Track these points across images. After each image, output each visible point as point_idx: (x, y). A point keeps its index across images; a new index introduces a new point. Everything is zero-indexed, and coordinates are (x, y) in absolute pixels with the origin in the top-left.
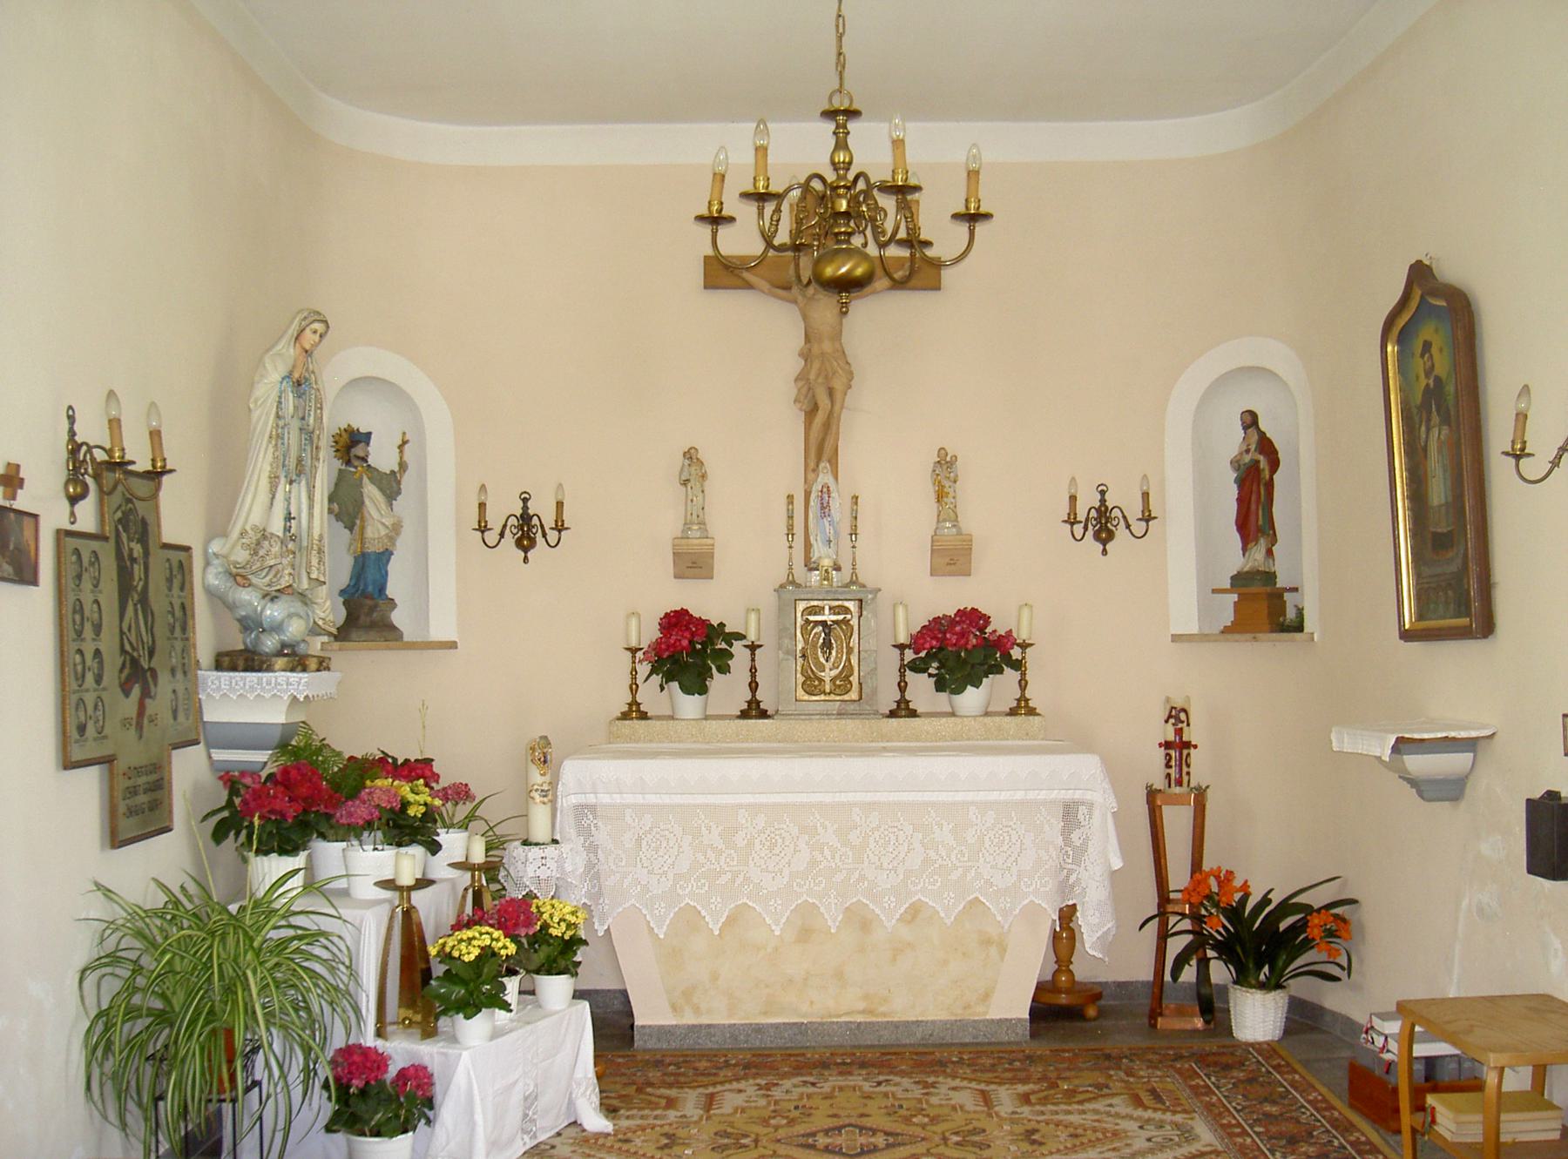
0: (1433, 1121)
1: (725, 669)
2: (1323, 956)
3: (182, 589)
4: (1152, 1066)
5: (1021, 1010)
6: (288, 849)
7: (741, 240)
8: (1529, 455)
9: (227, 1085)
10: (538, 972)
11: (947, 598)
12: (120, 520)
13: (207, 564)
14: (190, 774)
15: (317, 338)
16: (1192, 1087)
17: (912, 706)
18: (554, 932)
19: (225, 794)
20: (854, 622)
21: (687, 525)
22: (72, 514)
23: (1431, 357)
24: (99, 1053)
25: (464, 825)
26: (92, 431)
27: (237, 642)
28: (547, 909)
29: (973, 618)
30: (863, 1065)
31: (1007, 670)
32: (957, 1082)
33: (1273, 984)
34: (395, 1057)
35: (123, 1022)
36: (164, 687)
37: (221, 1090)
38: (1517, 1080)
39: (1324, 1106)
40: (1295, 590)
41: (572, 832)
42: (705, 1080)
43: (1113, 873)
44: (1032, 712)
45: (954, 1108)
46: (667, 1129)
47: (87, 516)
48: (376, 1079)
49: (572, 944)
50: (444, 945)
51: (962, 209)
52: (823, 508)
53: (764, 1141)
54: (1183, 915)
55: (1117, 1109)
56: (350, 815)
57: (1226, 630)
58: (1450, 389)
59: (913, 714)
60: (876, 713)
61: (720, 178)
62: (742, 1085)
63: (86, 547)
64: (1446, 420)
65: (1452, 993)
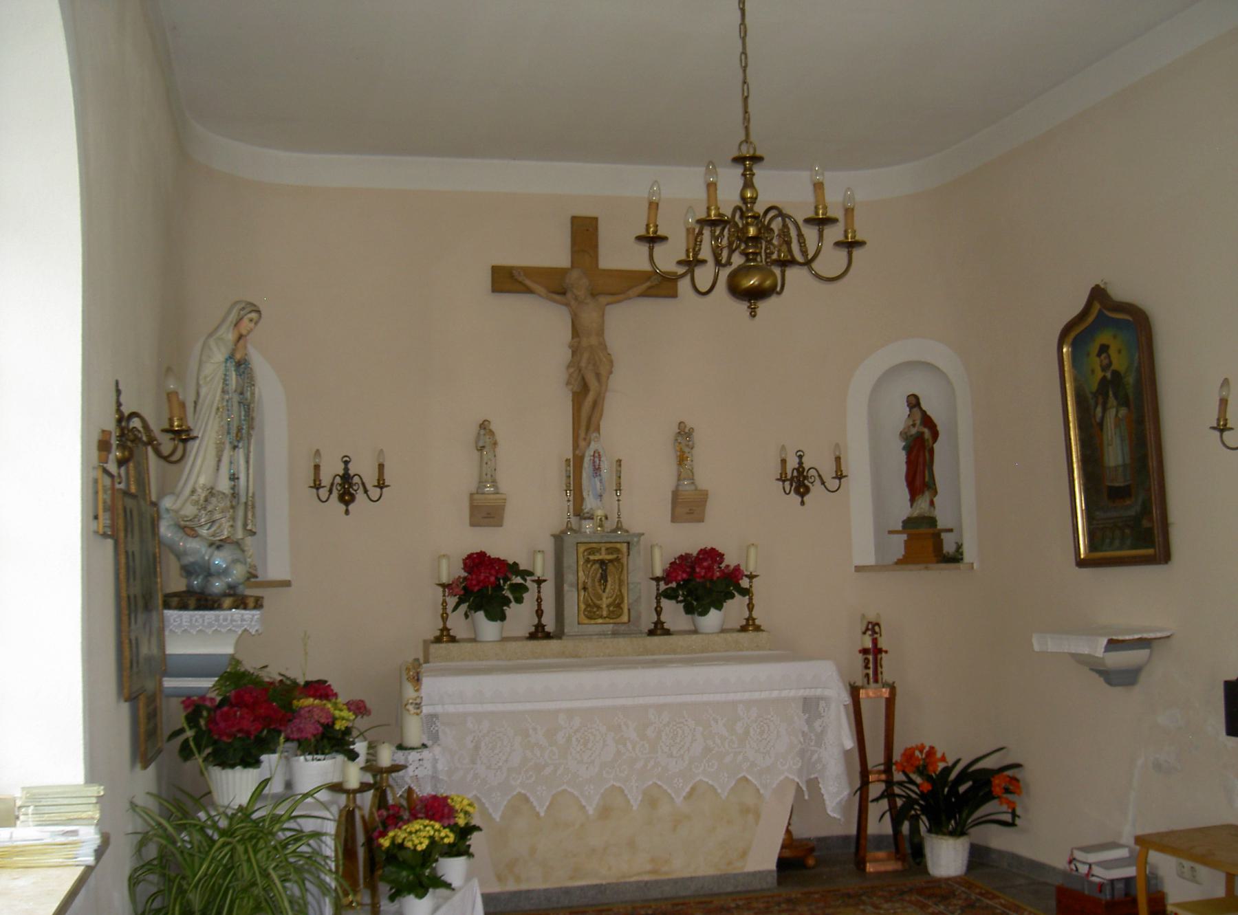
1: (519, 600)
5: (772, 865)
6: (251, 761)
11: (689, 540)
21: (481, 483)
23: (1109, 357)
29: (712, 555)
33: (959, 832)
44: (758, 629)
57: (899, 562)
59: (667, 632)
60: (641, 633)
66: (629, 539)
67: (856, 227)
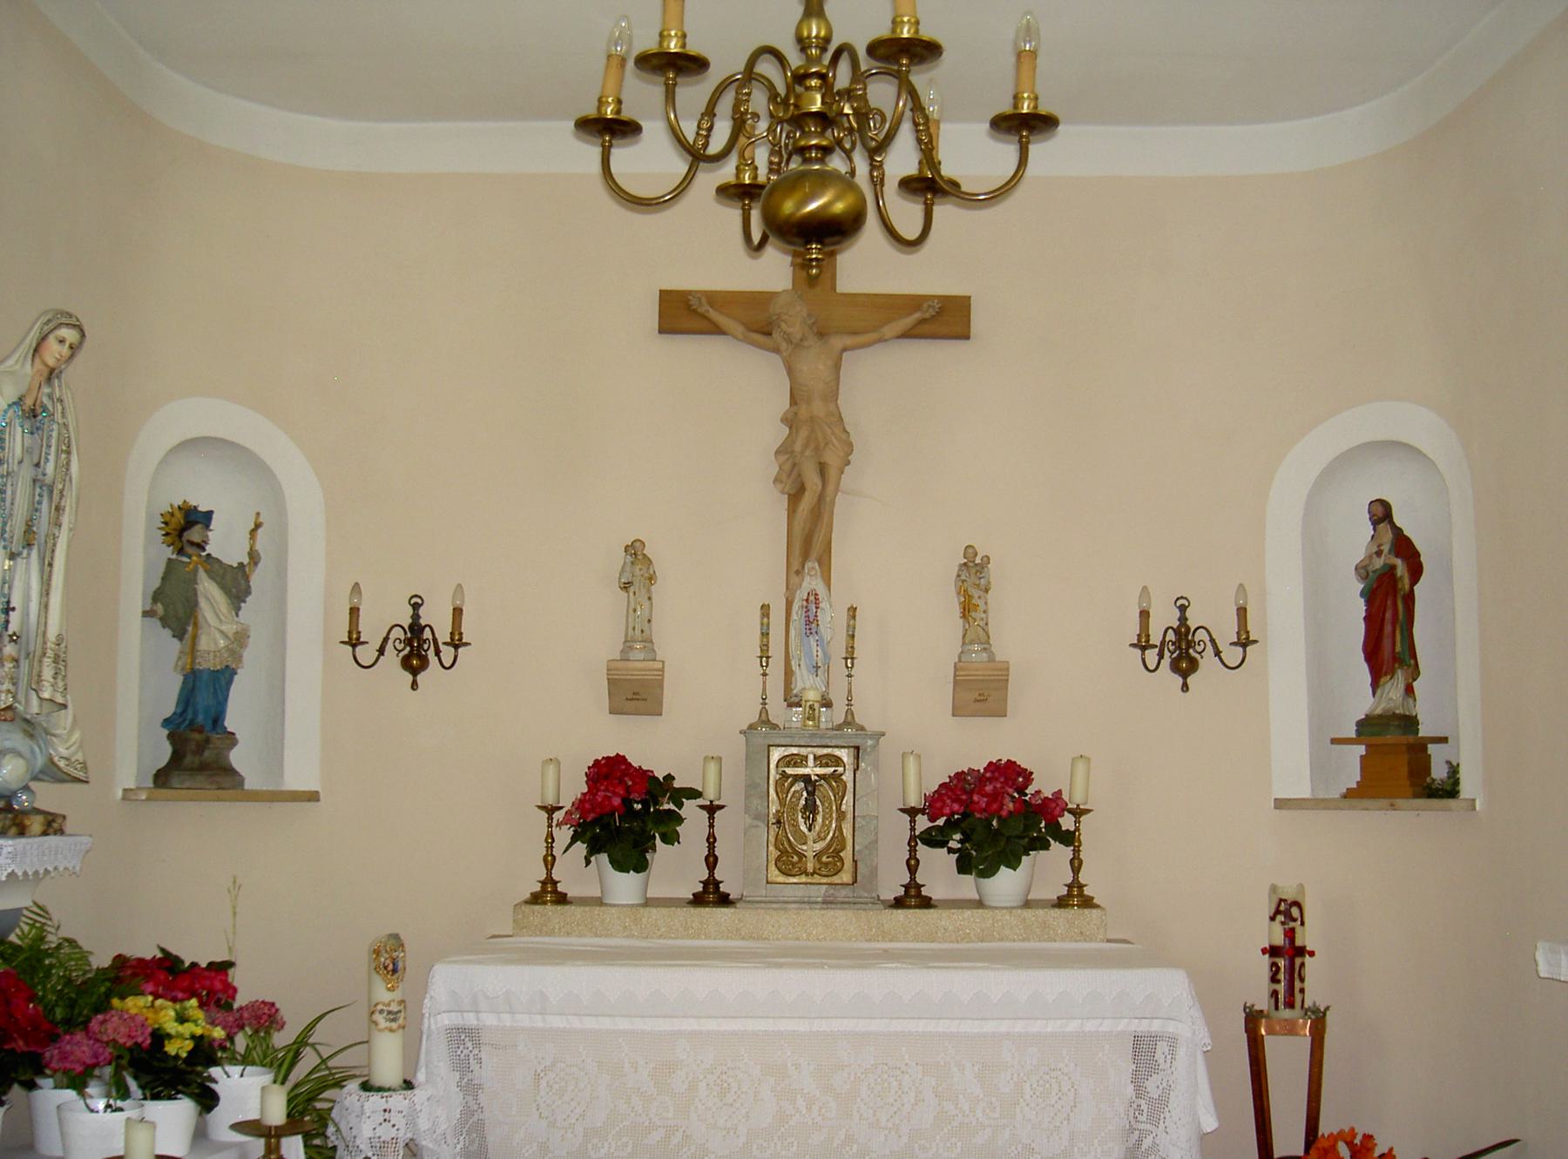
1: (671, 838)
11: (974, 747)
15: (65, 350)
20: (848, 777)
29: (1009, 774)
43: (1204, 1137)
44: (1087, 903)
52: (809, 622)
57: (1349, 794)
59: (927, 903)
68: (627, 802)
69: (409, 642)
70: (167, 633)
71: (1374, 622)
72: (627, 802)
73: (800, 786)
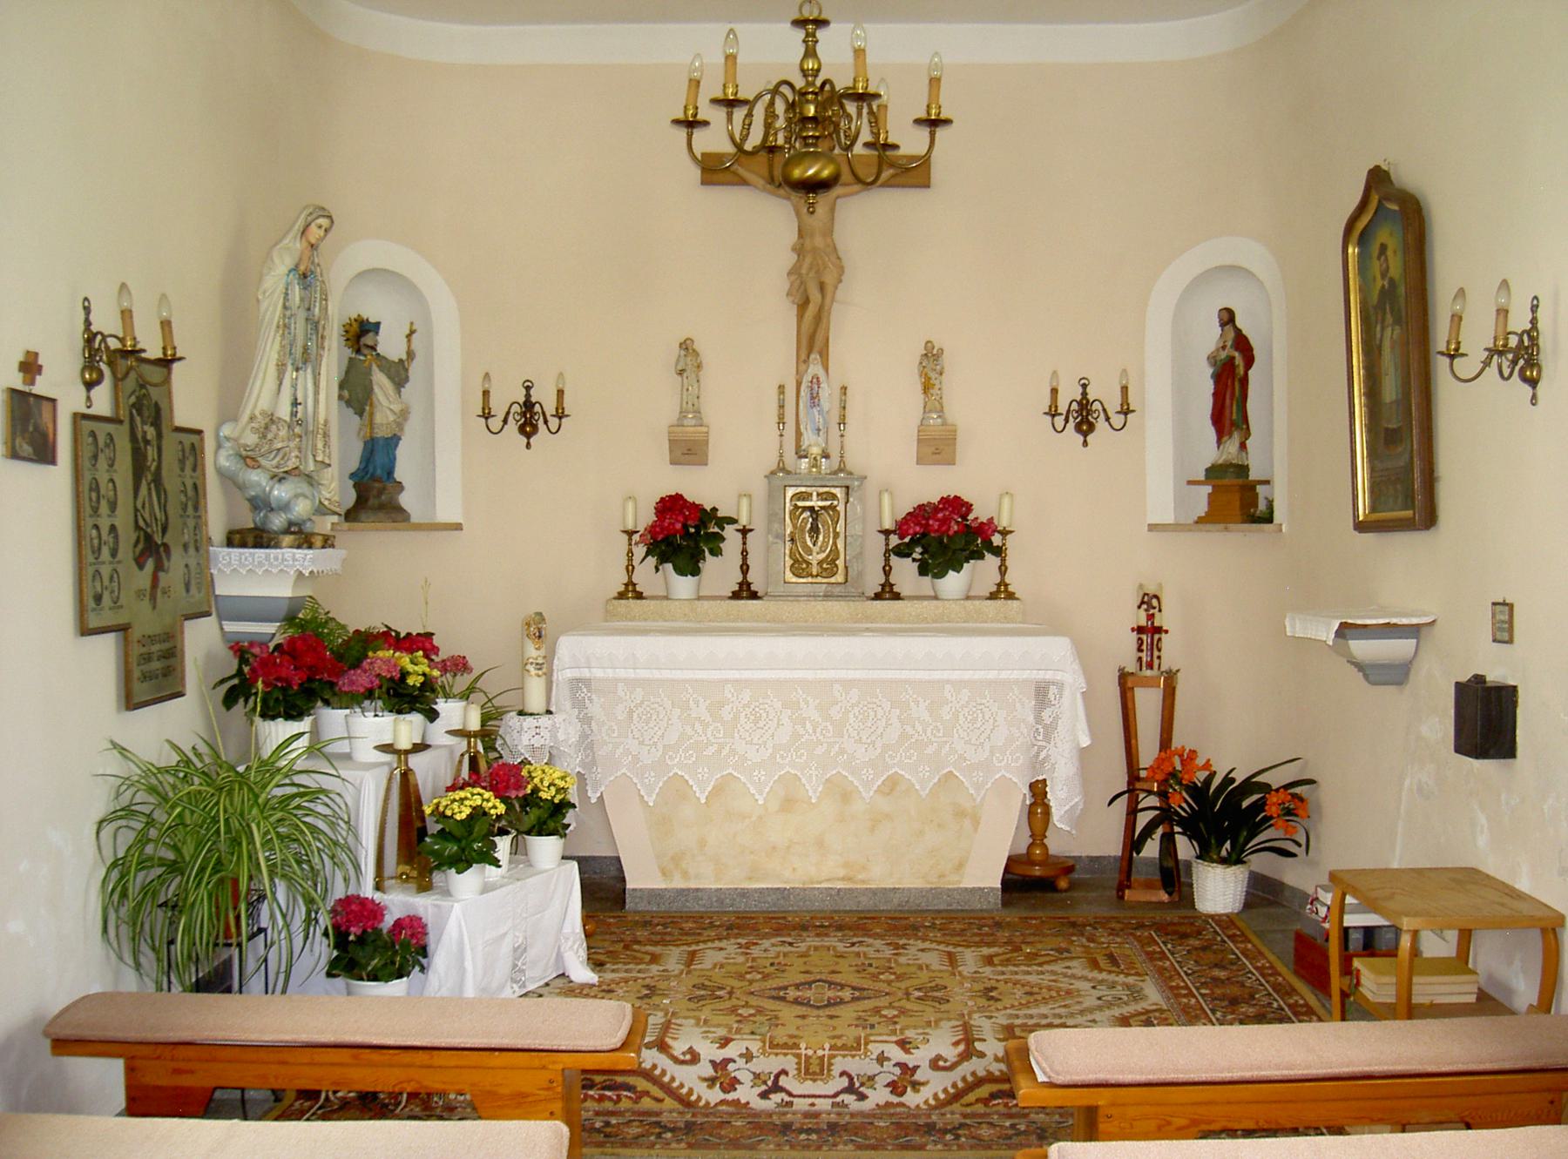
0: (1358, 983)
1: (716, 552)
2: (1279, 834)
3: (194, 470)
4: (1113, 932)
5: (993, 879)
6: (294, 714)
7: (714, 140)
8: (1463, 355)
9: (233, 930)
10: (529, 833)
11: (931, 486)
12: (133, 405)
13: (219, 446)
14: (203, 644)
15: (322, 233)
16: (1148, 953)
17: (896, 589)
18: (544, 795)
19: (235, 663)
20: (841, 508)
21: (683, 414)
22: (89, 398)
24: (116, 897)
25: (465, 696)
26: (106, 322)
27: (247, 520)
28: (538, 774)
29: (956, 506)
30: (840, 928)
31: (988, 556)
32: (927, 945)
33: (1234, 859)
34: (393, 909)
35: (138, 870)
36: (177, 562)
37: (227, 935)
38: (1438, 946)
39: (1269, 972)
40: (1267, 482)
41: (568, 705)
42: (690, 939)
43: (1083, 752)
44: (1011, 596)
45: (920, 968)
46: (648, 981)
47: (102, 401)
48: (375, 929)
49: (560, 808)
50: (438, 805)
51: (923, 115)
52: (812, 398)
53: (738, 993)
54: (1150, 792)
55: (1074, 971)
56: (352, 683)
57: (1200, 521)
58: (1401, 290)
59: (897, 597)
61: (695, 84)
62: (723, 944)
63: (103, 430)
64: (1398, 321)
65: (1395, 866)
66: (848, 483)
67: (941, 101)
68: (685, 526)
69: (524, 415)
70: (351, 411)
71: (1219, 396)
72: (685, 526)
73: (807, 514)
